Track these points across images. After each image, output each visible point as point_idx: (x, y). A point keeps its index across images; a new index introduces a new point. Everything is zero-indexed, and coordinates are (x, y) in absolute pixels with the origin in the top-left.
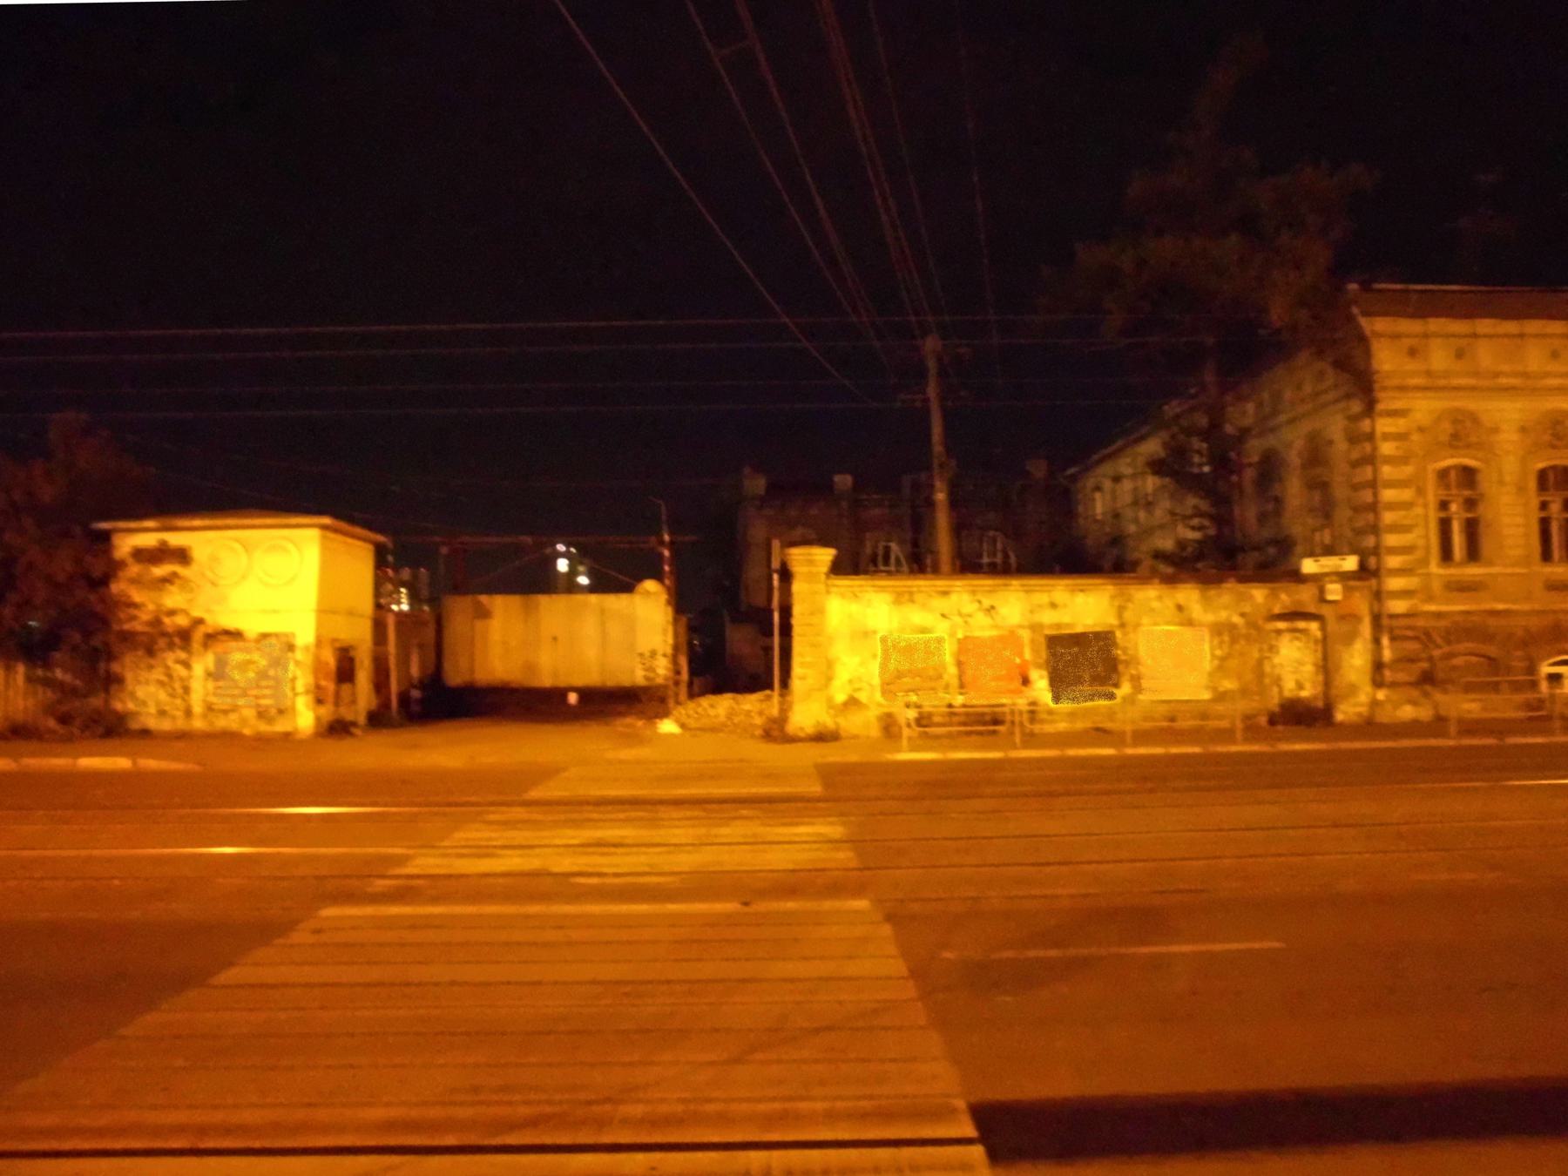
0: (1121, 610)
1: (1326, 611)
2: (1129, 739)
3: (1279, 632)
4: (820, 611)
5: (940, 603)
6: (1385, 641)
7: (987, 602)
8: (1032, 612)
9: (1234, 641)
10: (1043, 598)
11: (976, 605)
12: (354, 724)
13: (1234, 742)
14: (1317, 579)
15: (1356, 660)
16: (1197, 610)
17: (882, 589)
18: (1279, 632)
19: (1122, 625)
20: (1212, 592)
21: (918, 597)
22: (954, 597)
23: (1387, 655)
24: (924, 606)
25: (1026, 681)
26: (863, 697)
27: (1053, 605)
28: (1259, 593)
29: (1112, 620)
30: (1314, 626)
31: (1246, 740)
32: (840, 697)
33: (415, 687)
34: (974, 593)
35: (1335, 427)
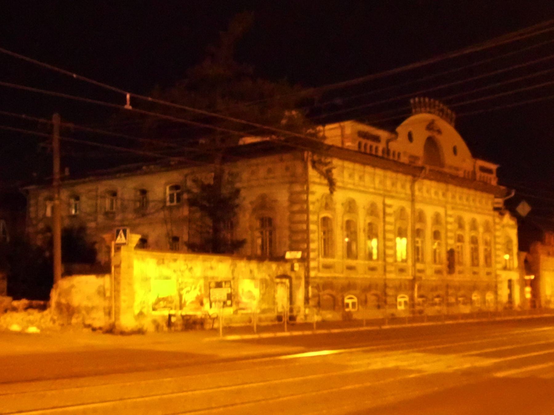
0: (233, 271)
1: (293, 275)
2: (315, 326)
3: (277, 283)
4: (130, 267)
5: (173, 265)
6: (310, 289)
7: (190, 266)
8: (205, 271)
9: (267, 287)
10: (208, 264)
11: (186, 267)
12: (156, 278)
13: (283, 330)
14: (291, 261)
15: (300, 296)
16: (256, 271)
17: (153, 257)
18: (277, 283)
19: (233, 278)
20: (261, 265)
21: (166, 262)
22: (178, 262)
23: (310, 294)
24: (168, 267)
25: (202, 304)
26: (145, 311)
27: (212, 268)
28: (274, 266)
29: (230, 276)
30: (287, 281)
31: (289, 330)
32: (137, 312)
33: (124, 244)
34: (185, 260)
35: (282, 197)
